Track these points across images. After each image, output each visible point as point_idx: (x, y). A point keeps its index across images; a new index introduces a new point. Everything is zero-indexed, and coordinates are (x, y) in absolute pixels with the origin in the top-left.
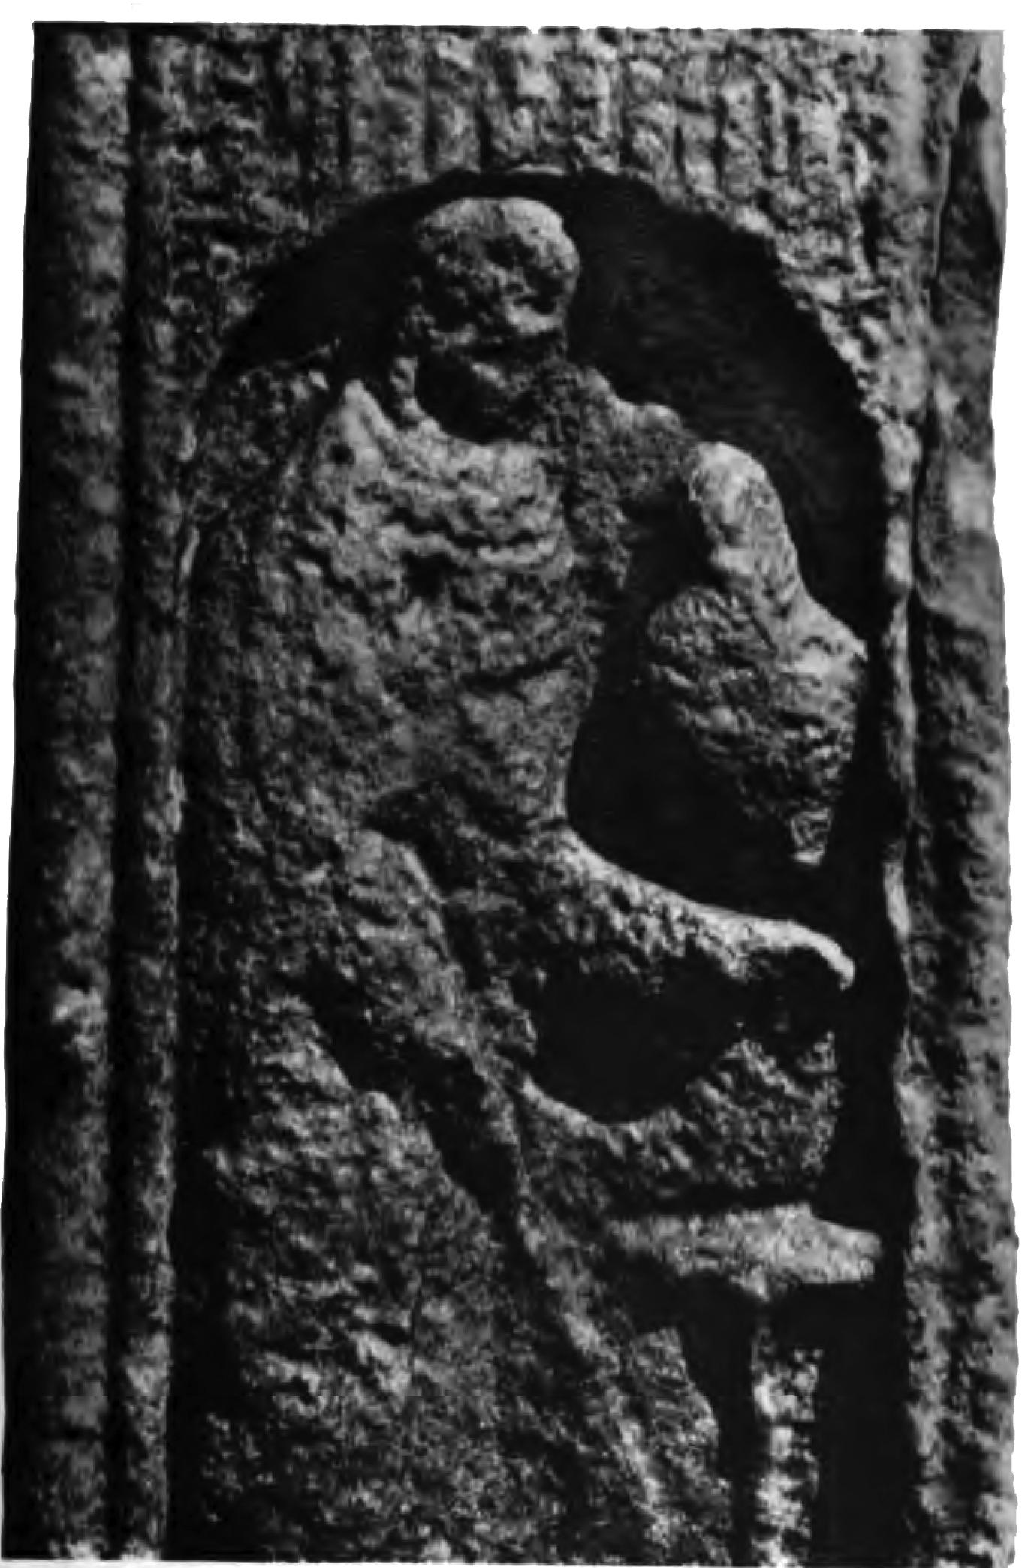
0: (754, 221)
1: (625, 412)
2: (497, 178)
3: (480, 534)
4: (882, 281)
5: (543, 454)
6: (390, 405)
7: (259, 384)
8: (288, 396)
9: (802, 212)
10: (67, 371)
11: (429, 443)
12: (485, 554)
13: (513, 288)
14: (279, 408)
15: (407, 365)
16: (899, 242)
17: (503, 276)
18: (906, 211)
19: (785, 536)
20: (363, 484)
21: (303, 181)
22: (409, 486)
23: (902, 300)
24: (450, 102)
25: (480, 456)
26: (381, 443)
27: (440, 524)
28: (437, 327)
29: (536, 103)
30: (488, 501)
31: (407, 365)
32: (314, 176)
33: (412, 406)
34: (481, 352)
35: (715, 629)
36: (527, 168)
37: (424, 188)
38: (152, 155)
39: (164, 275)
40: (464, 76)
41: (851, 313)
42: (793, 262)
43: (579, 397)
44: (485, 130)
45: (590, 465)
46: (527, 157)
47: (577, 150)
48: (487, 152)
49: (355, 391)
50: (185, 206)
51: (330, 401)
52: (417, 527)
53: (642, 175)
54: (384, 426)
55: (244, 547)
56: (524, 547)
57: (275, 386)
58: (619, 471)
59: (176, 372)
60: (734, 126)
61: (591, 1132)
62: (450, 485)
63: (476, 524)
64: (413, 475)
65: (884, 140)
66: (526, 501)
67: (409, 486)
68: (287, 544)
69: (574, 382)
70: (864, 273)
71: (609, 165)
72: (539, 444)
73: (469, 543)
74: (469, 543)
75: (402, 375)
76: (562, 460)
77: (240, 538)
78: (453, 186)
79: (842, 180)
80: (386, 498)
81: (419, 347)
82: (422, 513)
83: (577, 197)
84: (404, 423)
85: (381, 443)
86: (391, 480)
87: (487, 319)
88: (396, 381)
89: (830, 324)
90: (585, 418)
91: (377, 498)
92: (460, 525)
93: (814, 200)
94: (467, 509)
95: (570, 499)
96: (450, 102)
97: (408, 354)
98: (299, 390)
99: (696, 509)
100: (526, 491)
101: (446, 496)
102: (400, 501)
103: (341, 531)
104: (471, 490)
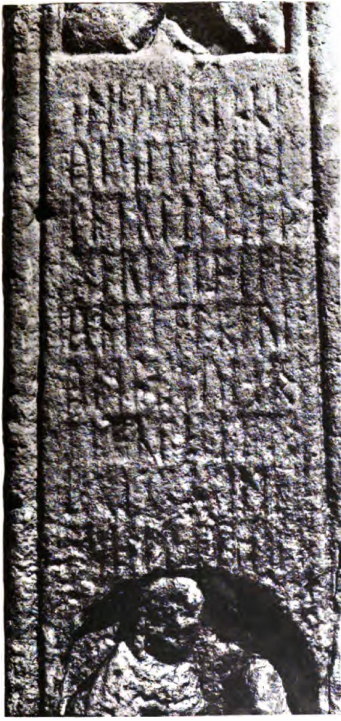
0: (268, 581)
1: (222, 647)
2: (172, 571)
3: (170, 699)
4: (313, 601)
5: (193, 666)
6: (136, 653)
7: (87, 644)
8: (98, 649)
9: (284, 577)
10: (17, 647)
11: (151, 666)
12: (172, 706)
13: (179, 610)
14: (95, 653)
15: (141, 639)
16: (321, 586)
17: (175, 606)
18: (322, 575)
19: (282, 689)
20: (126, 684)
21: (101, 575)
22: (142, 683)
23: (322, 607)
24: (154, 543)
25: (168, 669)
26: (133, 668)
27: (154, 696)
28: (152, 624)
29: (186, 542)
30: (171, 686)
31: (141, 639)
32: (105, 574)
33: (143, 653)
34: (168, 633)
35: (289, 491)
36: (184, 567)
37: (145, 576)
38: (46, 567)
39: (52, 612)
40: (159, 534)
41: (304, 613)
42: (282, 596)
43: (204, 644)
44: (168, 554)
45: (209, 669)
46: (183, 563)
47: (201, 559)
48: (168, 562)
49: (123, 646)
50: (58, 586)
51: (113, 651)
52: (146, 698)
53: (225, 567)
54: (133, 661)
55: (83, 708)
56: (186, 701)
57: (92, 645)
58: (220, 670)
59: (56, 647)
60: (259, 547)
61: (250, 408)
62: (158, 682)
63: (168, 696)
64: (144, 679)
65: (314, 550)
66: (186, 684)
67: (142, 683)
68: (99, 707)
69: (203, 639)
70: (308, 598)
71: (213, 564)
72: (190, 662)
73: (166, 702)
74: (166, 702)
75: (140, 642)
76: (199, 667)
77: (82, 704)
78: (155, 574)
79: (300, 564)
80: (134, 689)
81: (145, 631)
82: (148, 693)
83: (201, 576)
84: (141, 660)
85: (133, 668)
86: (137, 682)
87: (170, 622)
88: (138, 645)
89: (296, 618)
90: (207, 651)
91: (131, 688)
92: (163, 696)
93: (289, 573)
94: (164, 690)
95: (202, 681)
96: (154, 543)
97: (142, 635)
98: (102, 646)
99: (249, 687)
100: (186, 680)
101: (156, 686)
102: (139, 689)
103: (119, 702)
104: (164, 682)
